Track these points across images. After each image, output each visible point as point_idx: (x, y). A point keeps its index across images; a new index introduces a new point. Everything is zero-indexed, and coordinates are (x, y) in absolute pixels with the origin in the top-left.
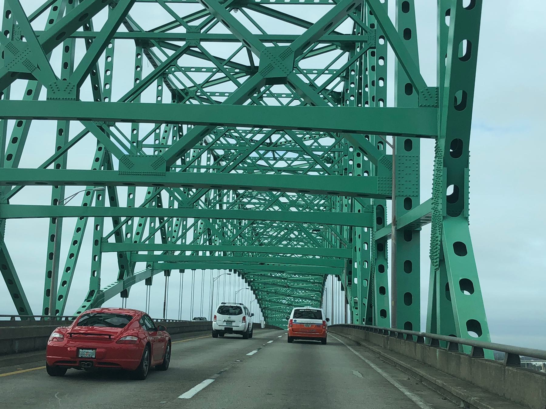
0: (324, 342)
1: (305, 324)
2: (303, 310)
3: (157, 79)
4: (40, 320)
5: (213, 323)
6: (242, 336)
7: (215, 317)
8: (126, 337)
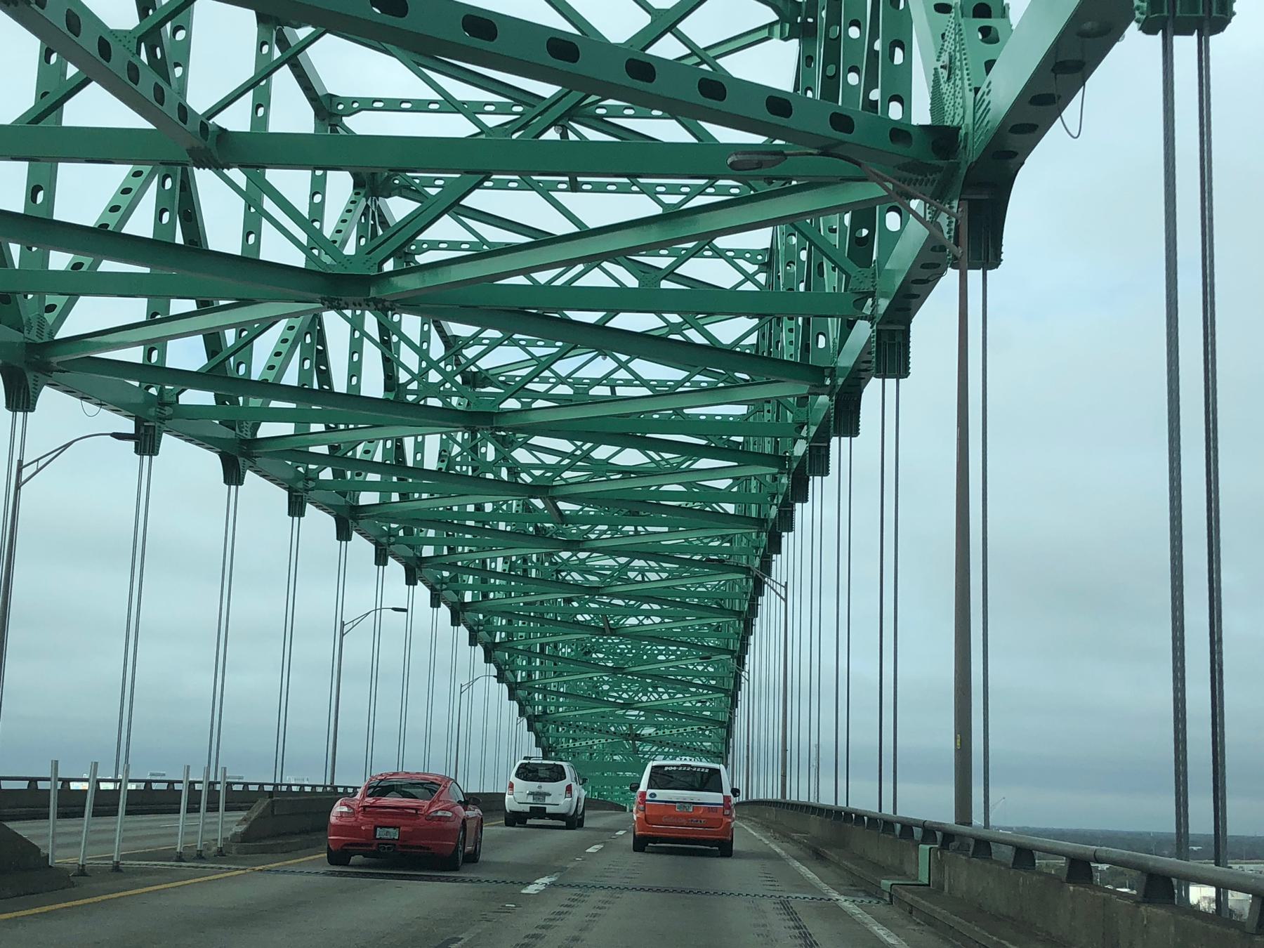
0: (724, 849)
1: (677, 804)
2: (673, 766)
3: (251, 91)
4: (241, 789)
5: (506, 797)
6: (564, 824)
7: (511, 786)
8: (437, 811)
